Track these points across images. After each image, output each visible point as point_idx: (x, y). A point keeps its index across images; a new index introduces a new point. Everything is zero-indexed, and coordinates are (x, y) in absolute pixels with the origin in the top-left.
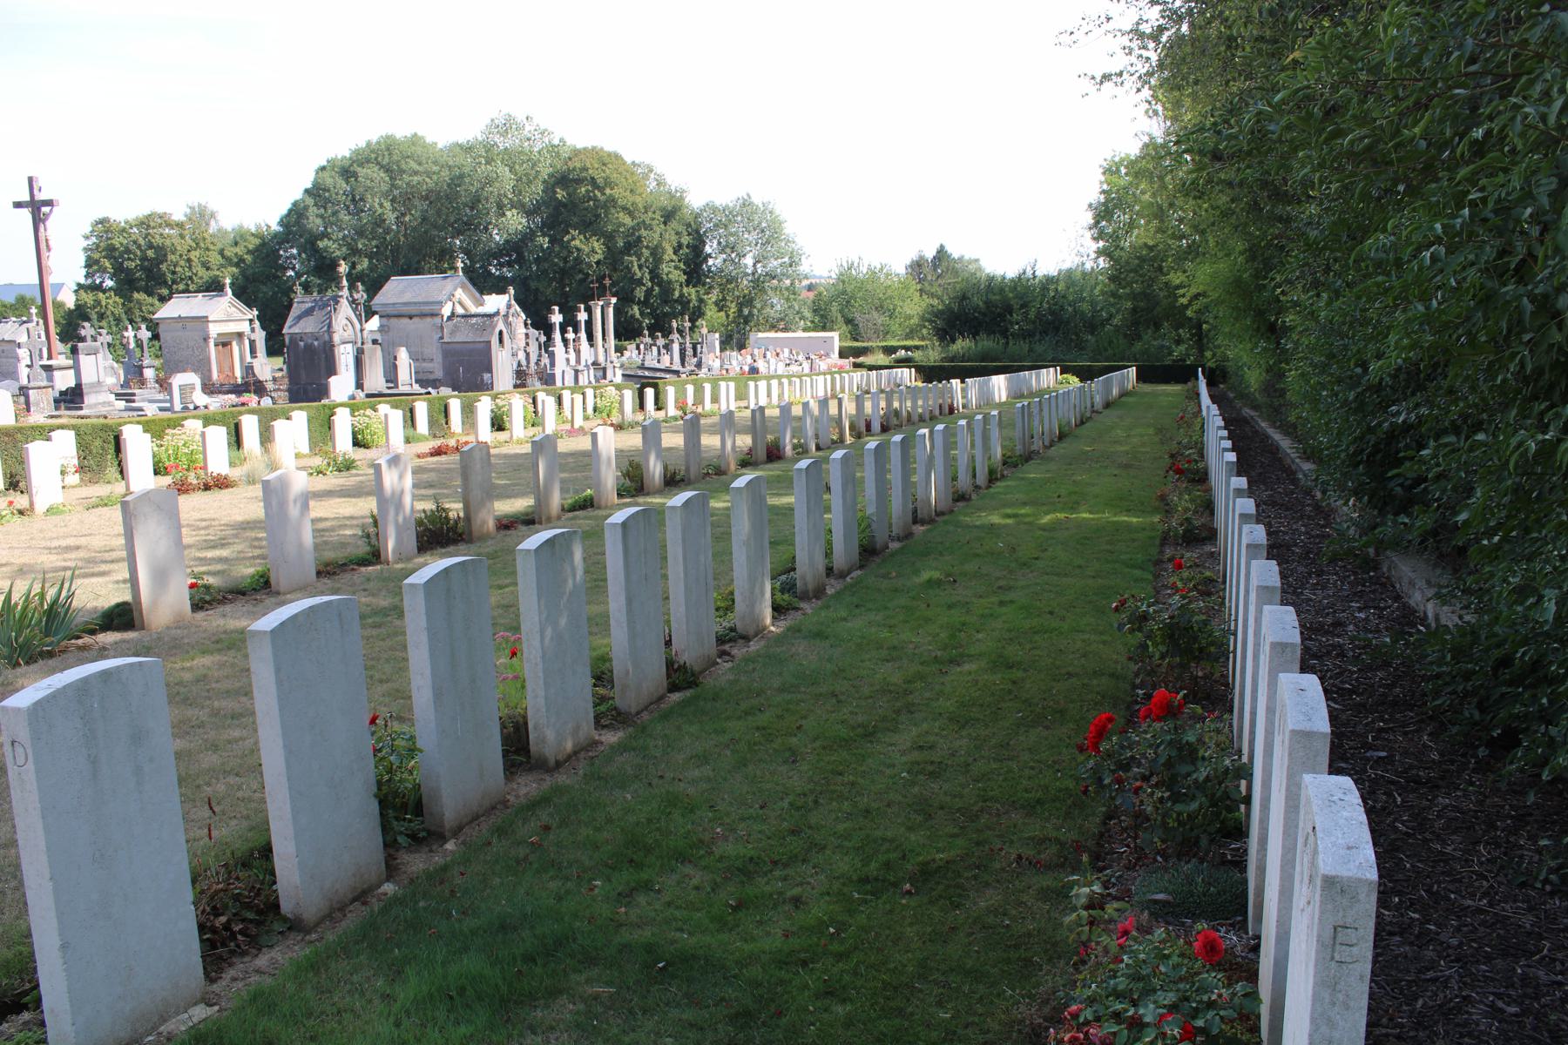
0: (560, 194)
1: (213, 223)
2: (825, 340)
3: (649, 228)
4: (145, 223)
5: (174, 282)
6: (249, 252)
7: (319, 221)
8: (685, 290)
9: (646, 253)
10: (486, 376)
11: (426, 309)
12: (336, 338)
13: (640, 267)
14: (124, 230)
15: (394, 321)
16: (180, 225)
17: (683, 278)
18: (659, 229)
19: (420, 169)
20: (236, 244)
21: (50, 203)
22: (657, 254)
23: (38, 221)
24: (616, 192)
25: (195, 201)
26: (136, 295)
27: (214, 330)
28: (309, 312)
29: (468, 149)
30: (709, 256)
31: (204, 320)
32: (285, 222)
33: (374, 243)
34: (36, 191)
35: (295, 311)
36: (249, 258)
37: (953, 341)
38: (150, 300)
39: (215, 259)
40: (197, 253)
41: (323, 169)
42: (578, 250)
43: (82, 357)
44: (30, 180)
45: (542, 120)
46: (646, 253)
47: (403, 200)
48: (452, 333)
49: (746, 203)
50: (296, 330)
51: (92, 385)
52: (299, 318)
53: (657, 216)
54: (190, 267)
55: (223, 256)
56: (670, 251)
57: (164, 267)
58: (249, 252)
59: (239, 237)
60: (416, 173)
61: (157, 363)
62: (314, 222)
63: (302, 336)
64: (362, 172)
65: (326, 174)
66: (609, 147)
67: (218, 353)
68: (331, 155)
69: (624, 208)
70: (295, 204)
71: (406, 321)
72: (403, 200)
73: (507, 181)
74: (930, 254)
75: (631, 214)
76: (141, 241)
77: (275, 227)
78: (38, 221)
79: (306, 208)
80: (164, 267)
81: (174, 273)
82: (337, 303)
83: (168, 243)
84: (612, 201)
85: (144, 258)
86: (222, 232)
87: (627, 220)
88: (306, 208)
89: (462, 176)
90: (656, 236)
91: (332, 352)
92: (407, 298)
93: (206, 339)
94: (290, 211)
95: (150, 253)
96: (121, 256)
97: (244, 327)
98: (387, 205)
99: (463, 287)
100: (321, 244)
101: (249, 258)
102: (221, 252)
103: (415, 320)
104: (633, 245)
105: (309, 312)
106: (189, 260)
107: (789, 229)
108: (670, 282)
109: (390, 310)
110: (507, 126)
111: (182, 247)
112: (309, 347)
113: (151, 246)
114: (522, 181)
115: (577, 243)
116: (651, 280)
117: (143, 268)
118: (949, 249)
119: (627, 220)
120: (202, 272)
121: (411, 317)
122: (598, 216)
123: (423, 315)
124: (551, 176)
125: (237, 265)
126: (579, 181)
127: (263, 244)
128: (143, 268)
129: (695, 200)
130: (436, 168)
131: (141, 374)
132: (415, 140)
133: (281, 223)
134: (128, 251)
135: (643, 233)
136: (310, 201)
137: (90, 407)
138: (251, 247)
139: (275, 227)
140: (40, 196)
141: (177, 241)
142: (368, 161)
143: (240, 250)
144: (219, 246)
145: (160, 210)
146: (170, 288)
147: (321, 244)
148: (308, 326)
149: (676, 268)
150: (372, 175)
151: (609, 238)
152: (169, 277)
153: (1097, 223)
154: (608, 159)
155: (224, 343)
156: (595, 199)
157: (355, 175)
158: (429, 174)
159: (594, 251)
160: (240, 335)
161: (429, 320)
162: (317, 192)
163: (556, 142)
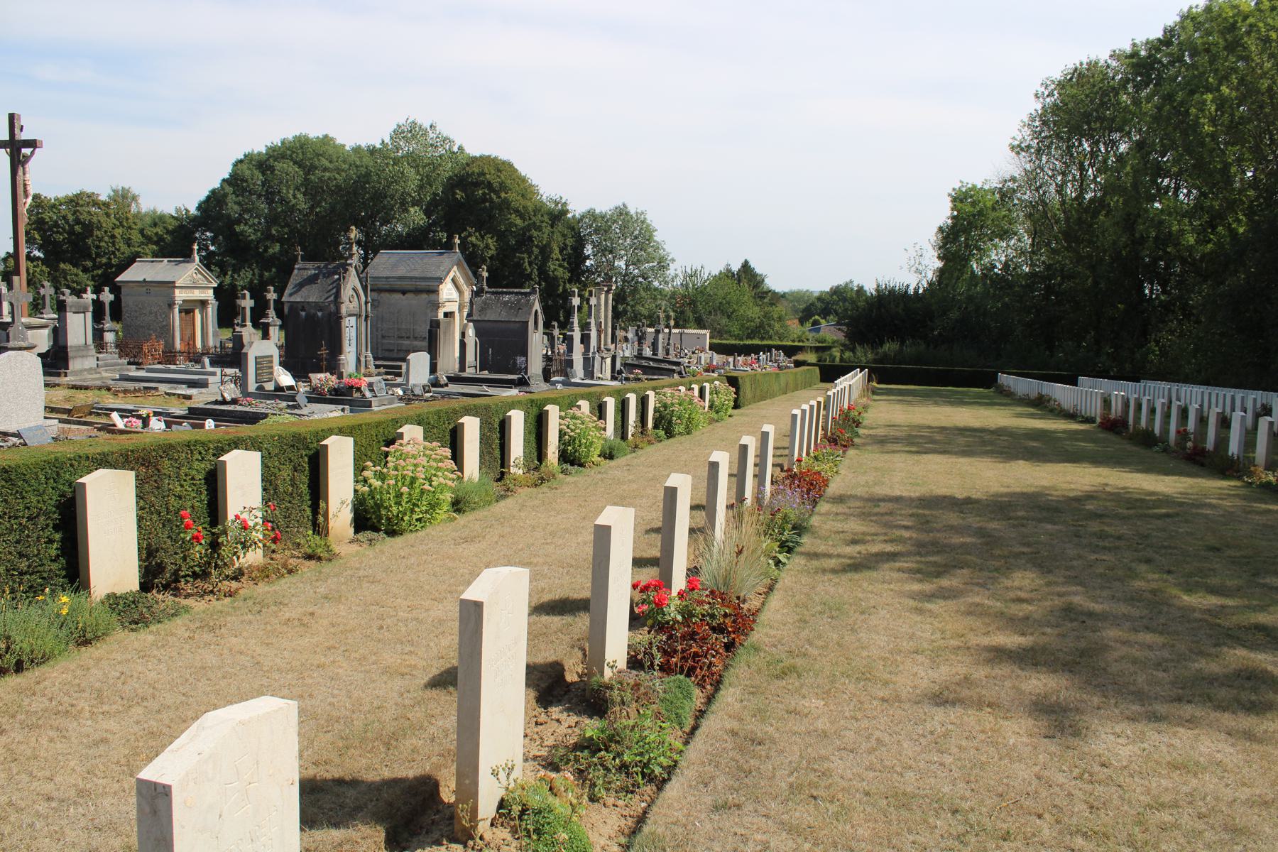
0: (459, 195)
1: (134, 205)
2: (698, 337)
3: (539, 229)
4: (75, 201)
5: (98, 255)
6: (168, 232)
7: (236, 207)
8: (568, 286)
9: (536, 251)
10: (520, 360)
11: (423, 284)
12: (344, 310)
13: (530, 264)
14: (54, 206)
15: (385, 296)
16: (106, 205)
17: (567, 275)
18: (547, 230)
19: (331, 166)
20: (155, 225)
21: (33, 144)
22: (545, 251)
23: (17, 163)
24: (511, 196)
25: (120, 184)
26: (62, 265)
27: (180, 296)
28: (312, 280)
29: (372, 151)
30: (588, 257)
31: (171, 285)
32: (205, 206)
33: (286, 230)
34: (17, 131)
35: (296, 277)
36: (168, 238)
37: (882, 344)
38: (75, 270)
39: (136, 237)
40: (120, 230)
41: (241, 161)
42: (474, 245)
43: (70, 316)
44: (12, 117)
45: (445, 129)
46: (536, 251)
47: (313, 191)
48: (482, 310)
49: (622, 212)
50: (292, 299)
51: (78, 348)
52: (300, 286)
53: (546, 218)
54: (113, 243)
55: (143, 235)
56: (557, 251)
57: (89, 241)
58: (168, 232)
59: (158, 220)
60: (325, 169)
61: (118, 326)
62: (232, 208)
63: (303, 306)
64: (278, 166)
65: (245, 167)
66: (503, 156)
67: (181, 318)
68: (248, 150)
69: (517, 211)
70: (213, 192)
71: (398, 296)
72: (313, 191)
73: (412, 179)
74: (736, 267)
75: (522, 217)
76: (71, 218)
77: (193, 210)
78: (17, 163)
79: (225, 195)
80: (89, 241)
81: (98, 247)
82: (346, 270)
83: (95, 220)
84: (506, 203)
85: (71, 232)
86: (138, 215)
87: (519, 222)
88: (225, 195)
89: (368, 174)
90: (545, 236)
91: (340, 324)
92: (402, 271)
93: (171, 305)
94: (208, 198)
95: (78, 228)
96: (50, 229)
97: (209, 295)
98: (300, 196)
99: (459, 265)
100: (237, 228)
101: (168, 238)
102: (142, 231)
103: (408, 295)
104: (525, 240)
105: (312, 280)
106: (113, 237)
107: (658, 237)
108: (556, 278)
109: (381, 284)
110: (411, 132)
111: (107, 224)
112: (311, 318)
113: (78, 221)
114: (426, 182)
115: (473, 239)
116: (539, 275)
117: (70, 242)
118: (752, 264)
119: (519, 222)
120: (123, 247)
121: (404, 293)
122: (491, 217)
123: (417, 291)
124: (450, 178)
125: (156, 243)
126: (477, 185)
127: (181, 227)
128: (70, 242)
129: (577, 208)
130: (345, 166)
131: (102, 338)
132: (326, 140)
133: (199, 208)
134: (56, 224)
135: (535, 233)
136: (229, 189)
137: (75, 373)
138: (170, 228)
139: (193, 210)
140: (24, 136)
141: (103, 219)
142: (283, 157)
143: (159, 230)
144: (139, 226)
145: (89, 190)
146: (94, 260)
147: (237, 228)
148: (312, 295)
149: (560, 266)
150: (285, 167)
151: (501, 237)
152: (94, 250)
153: (945, 244)
154: (503, 167)
155: (188, 310)
156: (491, 201)
157: (272, 169)
158: (339, 171)
159: (487, 247)
160: (203, 303)
161: (424, 296)
162: (235, 181)
163: (455, 149)
